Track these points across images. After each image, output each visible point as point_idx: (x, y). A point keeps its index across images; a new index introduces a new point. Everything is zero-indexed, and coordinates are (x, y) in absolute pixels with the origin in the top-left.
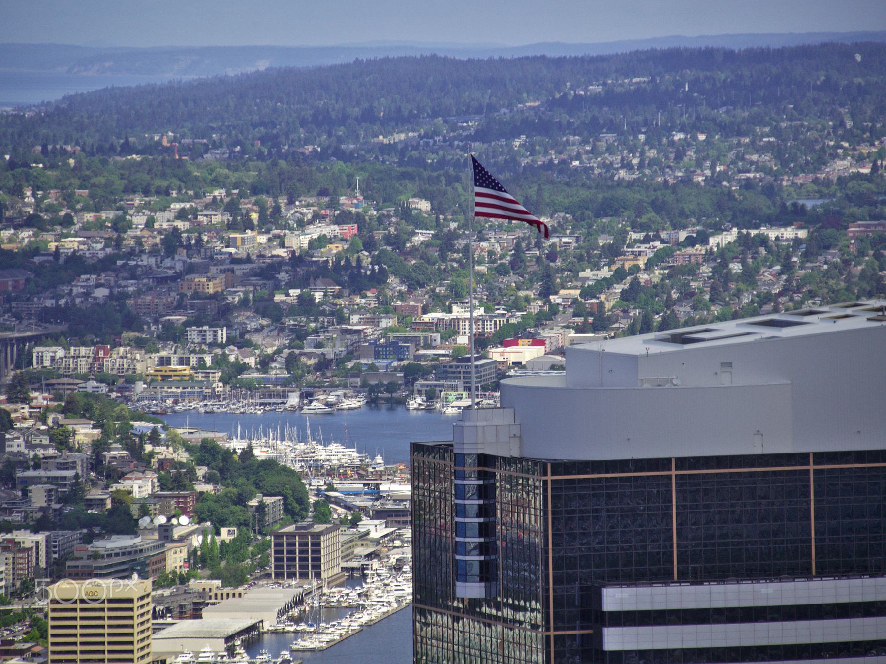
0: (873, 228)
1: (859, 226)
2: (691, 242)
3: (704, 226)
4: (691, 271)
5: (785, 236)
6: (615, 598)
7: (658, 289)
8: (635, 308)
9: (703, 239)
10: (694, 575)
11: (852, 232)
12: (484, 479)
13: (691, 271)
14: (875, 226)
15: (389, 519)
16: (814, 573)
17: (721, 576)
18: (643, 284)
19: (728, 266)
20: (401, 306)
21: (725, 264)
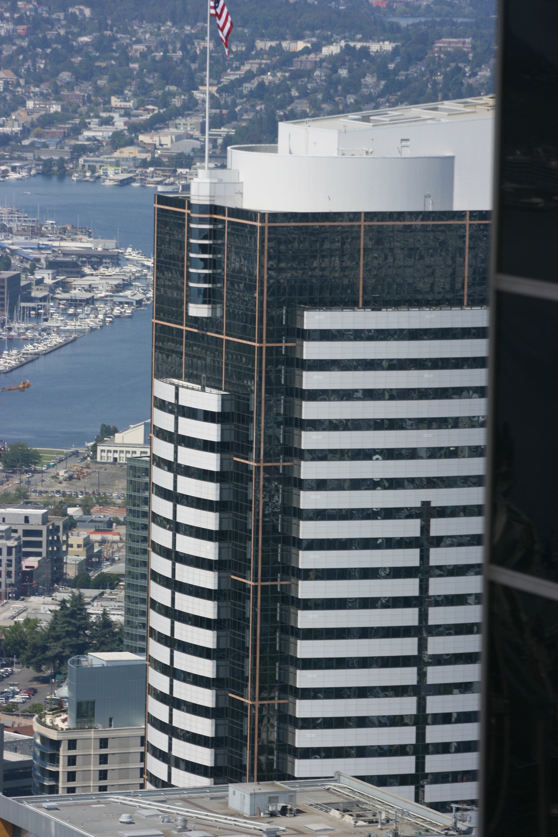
0: (452, 45)
1: (443, 43)
2: (306, 51)
3: (318, 38)
4: (309, 74)
5: (383, 48)
6: (313, 319)
7: (282, 87)
8: (261, 104)
9: (317, 48)
10: (375, 303)
11: (437, 47)
12: (214, 224)
13: (309, 74)
14: (456, 43)
15: (60, 269)
16: (465, 303)
17: (396, 304)
18: (267, 84)
19: (337, 71)
20: (68, 96)
21: (334, 70)
